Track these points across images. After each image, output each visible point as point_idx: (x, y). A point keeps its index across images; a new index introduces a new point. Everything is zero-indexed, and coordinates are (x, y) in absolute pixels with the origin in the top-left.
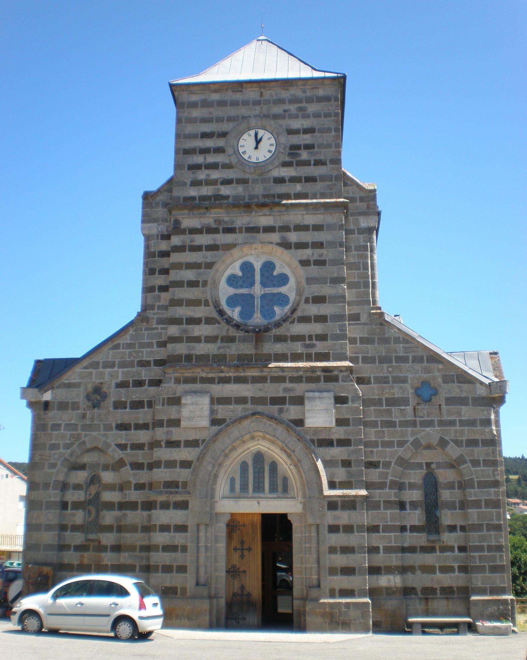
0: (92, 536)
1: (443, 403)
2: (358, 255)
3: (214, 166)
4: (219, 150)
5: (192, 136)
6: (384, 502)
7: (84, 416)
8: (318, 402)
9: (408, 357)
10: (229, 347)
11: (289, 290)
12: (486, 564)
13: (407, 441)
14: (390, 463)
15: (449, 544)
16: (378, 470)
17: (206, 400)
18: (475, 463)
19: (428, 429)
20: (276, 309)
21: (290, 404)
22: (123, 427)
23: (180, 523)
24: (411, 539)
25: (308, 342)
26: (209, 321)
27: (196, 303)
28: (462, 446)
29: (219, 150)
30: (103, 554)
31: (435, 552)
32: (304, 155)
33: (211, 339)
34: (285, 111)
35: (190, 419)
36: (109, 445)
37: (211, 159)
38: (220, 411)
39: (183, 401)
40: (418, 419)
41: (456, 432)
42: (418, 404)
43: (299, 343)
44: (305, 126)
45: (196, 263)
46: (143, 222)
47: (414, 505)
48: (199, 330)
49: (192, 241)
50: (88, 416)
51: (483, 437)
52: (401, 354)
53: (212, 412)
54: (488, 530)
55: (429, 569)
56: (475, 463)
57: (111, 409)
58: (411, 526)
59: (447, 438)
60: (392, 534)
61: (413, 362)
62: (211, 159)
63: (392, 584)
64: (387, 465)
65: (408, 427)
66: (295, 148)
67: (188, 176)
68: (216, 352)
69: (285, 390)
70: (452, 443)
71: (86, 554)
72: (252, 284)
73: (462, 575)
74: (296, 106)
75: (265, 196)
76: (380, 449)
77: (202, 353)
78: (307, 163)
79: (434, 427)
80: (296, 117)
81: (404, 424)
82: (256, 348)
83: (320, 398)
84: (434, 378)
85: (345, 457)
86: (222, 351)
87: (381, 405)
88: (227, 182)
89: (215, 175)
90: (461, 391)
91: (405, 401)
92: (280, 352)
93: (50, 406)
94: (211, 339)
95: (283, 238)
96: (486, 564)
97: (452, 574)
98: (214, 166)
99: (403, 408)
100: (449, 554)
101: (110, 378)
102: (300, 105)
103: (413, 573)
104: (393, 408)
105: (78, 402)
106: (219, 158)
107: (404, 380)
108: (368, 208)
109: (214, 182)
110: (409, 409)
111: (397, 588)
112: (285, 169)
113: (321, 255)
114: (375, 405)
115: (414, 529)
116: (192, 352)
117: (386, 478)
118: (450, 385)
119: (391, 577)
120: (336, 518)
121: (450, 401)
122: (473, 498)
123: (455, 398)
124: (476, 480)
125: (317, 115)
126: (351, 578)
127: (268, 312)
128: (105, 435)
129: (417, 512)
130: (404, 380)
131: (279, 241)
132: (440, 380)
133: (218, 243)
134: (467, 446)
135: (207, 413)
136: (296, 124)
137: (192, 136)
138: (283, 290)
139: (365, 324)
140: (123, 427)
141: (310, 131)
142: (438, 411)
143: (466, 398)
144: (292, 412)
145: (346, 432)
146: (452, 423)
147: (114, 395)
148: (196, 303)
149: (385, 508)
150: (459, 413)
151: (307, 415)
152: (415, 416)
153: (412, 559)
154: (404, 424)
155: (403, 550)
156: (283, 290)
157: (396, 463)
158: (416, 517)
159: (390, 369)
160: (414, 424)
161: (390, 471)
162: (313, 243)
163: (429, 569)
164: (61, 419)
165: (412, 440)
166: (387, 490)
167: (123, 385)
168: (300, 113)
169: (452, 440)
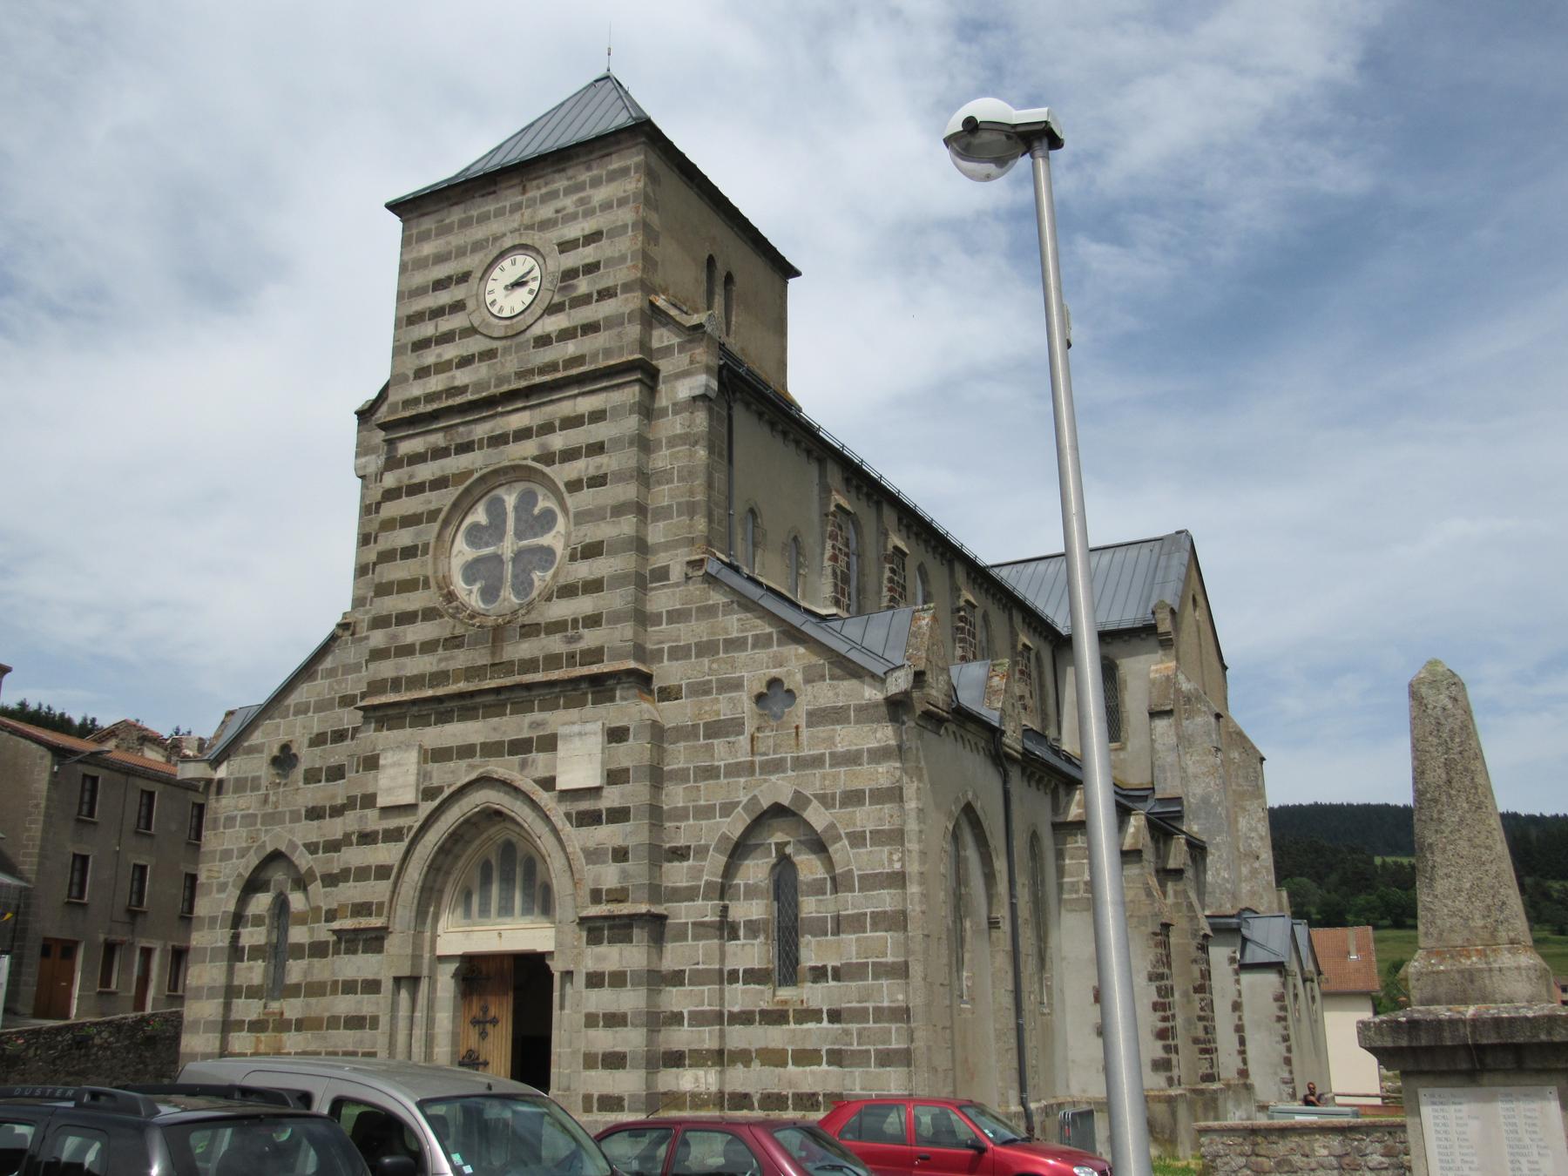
0: (275, 1006)
1: (803, 723)
2: (671, 455)
3: (446, 338)
4: (458, 306)
5: (420, 292)
6: (694, 924)
7: (266, 801)
8: (577, 742)
9: (746, 638)
10: (452, 658)
11: (462, 551)
12: (872, 1048)
13: (738, 803)
14: (706, 849)
15: (814, 1005)
16: (685, 864)
17: (412, 757)
18: (857, 839)
19: (773, 778)
20: (537, 575)
21: (538, 751)
22: (315, 814)
23: (370, 977)
24: (739, 997)
25: (570, 633)
26: (430, 614)
27: (408, 586)
28: (833, 806)
29: (458, 306)
30: (285, 1036)
31: (788, 1022)
32: (583, 285)
33: (429, 647)
34: (557, 211)
35: (389, 790)
36: (293, 846)
37: (447, 324)
38: (435, 775)
39: (382, 762)
40: (757, 759)
41: (824, 778)
42: (758, 729)
43: (558, 636)
44: (587, 232)
45: (415, 515)
46: (358, 455)
47: (753, 928)
48: (415, 633)
49: (411, 477)
50: (272, 798)
51: (874, 785)
52: (735, 635)
53: (423, 775)
54: (876, 977)
55: (774, 1058)
56: (857, 839)
57: (301, 784)
58: (745, 971)
59: (808, 793)
60: (706, 988)
61: (754, 646)
62: (447, 324)
63: (703, 1088)
64: (702, 851)
65: (739, 776)
66: (570, 274)
67: (412, 362)
68: (435, 669)
69: (535, 725)
70: (815, 803)
71: (262, 1036)
72: (501, 536)
73: (834, 1069)
74: (575, 197)
75: (520, 375)
76: (691, 822)
77: (415, 672)
78: (585, 300)
79: (784, 771)
80: (573, 217)
81: (735, 770)
82: (493, 654)
83: (580, 734)
84: (789, 673)
85: (619, 842)
86: (443, 666)
87: (697, 737)
88: (465, 362)
89: (450, 352)
90: (837, 695)
91: (735, 726)
92: (528, 656)
93: (225, 786)
94: (429, 647)
95: (542, 446)
96: (872, 1048)
97: (815, 1068)
98: (446, 338)
99: (732, 739)
100: (811, 1025)
101: (294, 729)
102: (582, 195)
103: (747, 1064)
104: (716, 741)
105: (259, 778)
106: (455, 322)
107: (737, 685)
108: (692, 362)
109: (443, 367)
110: (743, 740)
111: (709, 1094)
112: (553, 318)
113: (599, 467)
114: (686, 738)
115: (753, 976)
116: (402, 673)
117: (700, 879)
118: (818, 685)
119: (701, 1072)
120: (600, 958)
121: (818, 717)
122: (849, 912)
123: (824, 710)
124: (856, 873)
125: (607, 206)
126: (619, 1074)
127: (522, 586)
128: (291, 831)
129: (756, 942)
130: (737, 685)
131: (536, 453)
132: (799, 677)
133: (448, 472)
134: (843, 804)
135: (412, 779)
136: (573, 231)
137: (420, 292)
138: (546, 540)
139: (677, 585)
140: (315, 814)
141: (593, 238)
142: (793, 742)
143: (846, 709)
144: (540, 763)
145: (622, 795)
146: (817, 761)
147: (308, 758)
148: (408, 586)
149: (695, 938)
150: (831, 740)
151: (559, 769)
152: (753, 753)
153: (739, 1038)
154: (735, 770)
155: (718, 1018)
156: (546, 540)
157: (717, 849)
158: (751, 953)
159: (715, 666)
160: (749, 769)
161: (706, 864)
162: (589, 447)
163: (774, 1058)
164: (236, 808)
165: (745, 800)
166: (700, 902)
167: (318, 740)
168: (580, 209)
169: (816, 796)
